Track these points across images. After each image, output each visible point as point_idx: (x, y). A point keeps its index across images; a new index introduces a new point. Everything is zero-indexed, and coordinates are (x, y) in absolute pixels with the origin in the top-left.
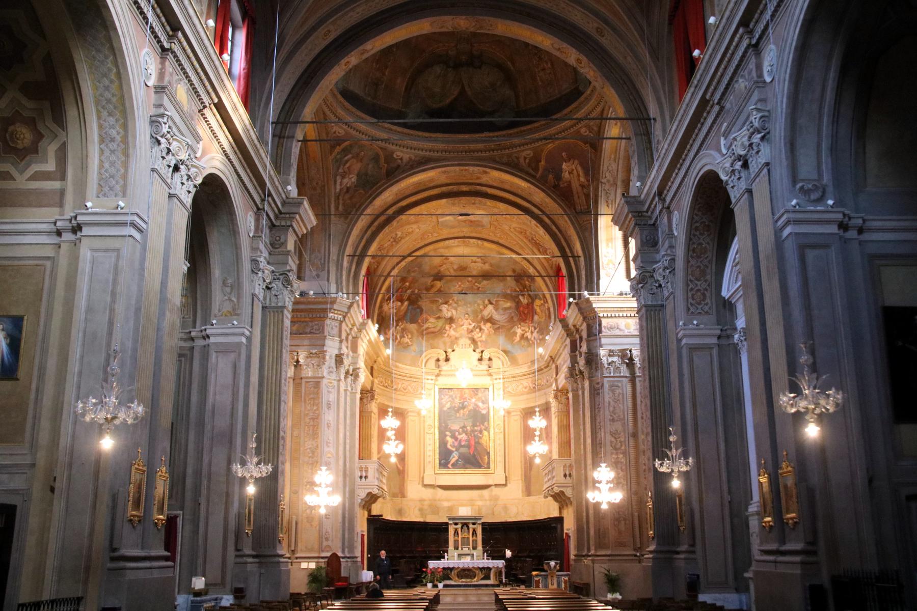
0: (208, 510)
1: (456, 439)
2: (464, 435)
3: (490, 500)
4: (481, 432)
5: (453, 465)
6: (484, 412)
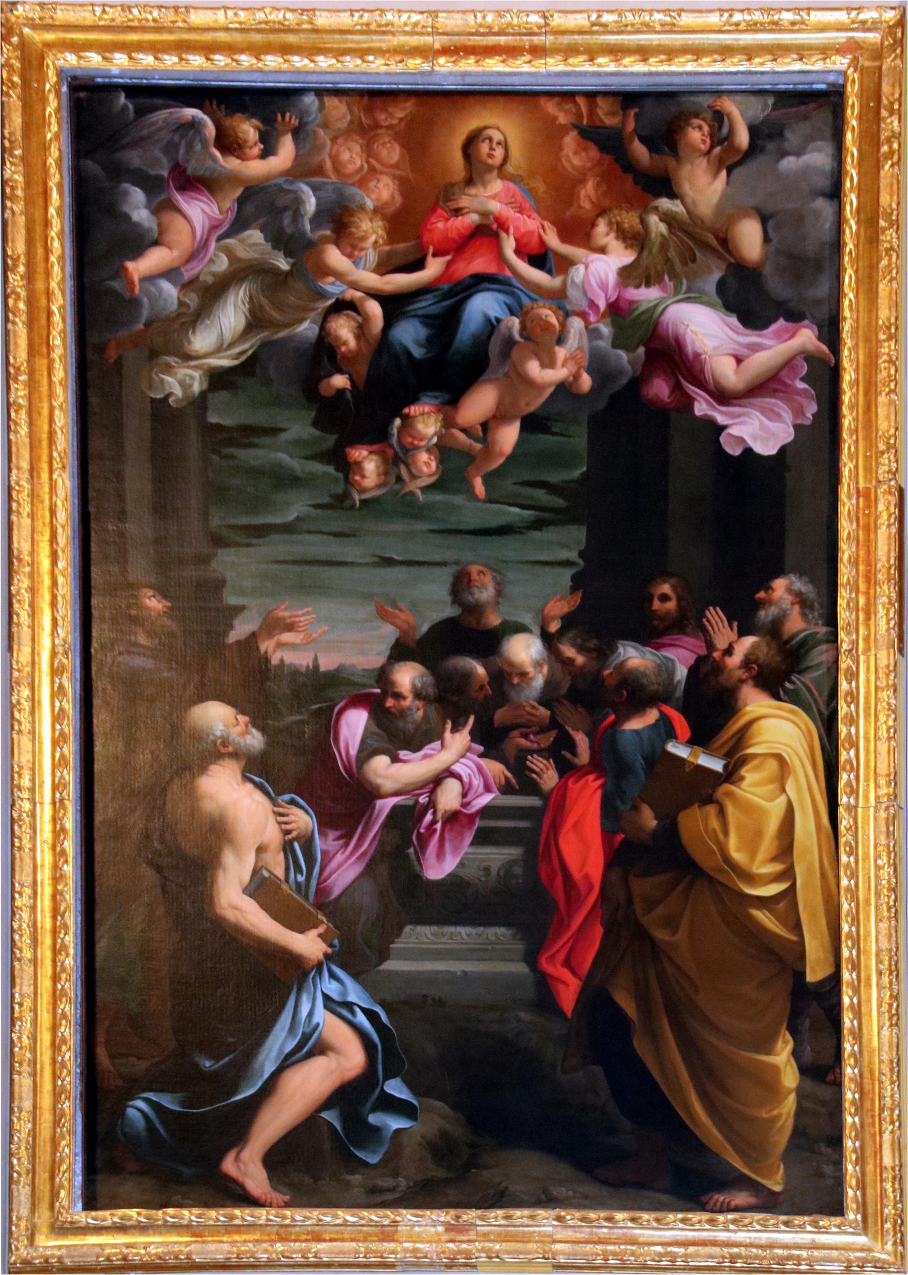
0: (34, 745)
1: (341, 798)
2: (455, 748)
3: (377, 126)
4: (709, 708)
5: (282, 1159)
6: (760, 431)
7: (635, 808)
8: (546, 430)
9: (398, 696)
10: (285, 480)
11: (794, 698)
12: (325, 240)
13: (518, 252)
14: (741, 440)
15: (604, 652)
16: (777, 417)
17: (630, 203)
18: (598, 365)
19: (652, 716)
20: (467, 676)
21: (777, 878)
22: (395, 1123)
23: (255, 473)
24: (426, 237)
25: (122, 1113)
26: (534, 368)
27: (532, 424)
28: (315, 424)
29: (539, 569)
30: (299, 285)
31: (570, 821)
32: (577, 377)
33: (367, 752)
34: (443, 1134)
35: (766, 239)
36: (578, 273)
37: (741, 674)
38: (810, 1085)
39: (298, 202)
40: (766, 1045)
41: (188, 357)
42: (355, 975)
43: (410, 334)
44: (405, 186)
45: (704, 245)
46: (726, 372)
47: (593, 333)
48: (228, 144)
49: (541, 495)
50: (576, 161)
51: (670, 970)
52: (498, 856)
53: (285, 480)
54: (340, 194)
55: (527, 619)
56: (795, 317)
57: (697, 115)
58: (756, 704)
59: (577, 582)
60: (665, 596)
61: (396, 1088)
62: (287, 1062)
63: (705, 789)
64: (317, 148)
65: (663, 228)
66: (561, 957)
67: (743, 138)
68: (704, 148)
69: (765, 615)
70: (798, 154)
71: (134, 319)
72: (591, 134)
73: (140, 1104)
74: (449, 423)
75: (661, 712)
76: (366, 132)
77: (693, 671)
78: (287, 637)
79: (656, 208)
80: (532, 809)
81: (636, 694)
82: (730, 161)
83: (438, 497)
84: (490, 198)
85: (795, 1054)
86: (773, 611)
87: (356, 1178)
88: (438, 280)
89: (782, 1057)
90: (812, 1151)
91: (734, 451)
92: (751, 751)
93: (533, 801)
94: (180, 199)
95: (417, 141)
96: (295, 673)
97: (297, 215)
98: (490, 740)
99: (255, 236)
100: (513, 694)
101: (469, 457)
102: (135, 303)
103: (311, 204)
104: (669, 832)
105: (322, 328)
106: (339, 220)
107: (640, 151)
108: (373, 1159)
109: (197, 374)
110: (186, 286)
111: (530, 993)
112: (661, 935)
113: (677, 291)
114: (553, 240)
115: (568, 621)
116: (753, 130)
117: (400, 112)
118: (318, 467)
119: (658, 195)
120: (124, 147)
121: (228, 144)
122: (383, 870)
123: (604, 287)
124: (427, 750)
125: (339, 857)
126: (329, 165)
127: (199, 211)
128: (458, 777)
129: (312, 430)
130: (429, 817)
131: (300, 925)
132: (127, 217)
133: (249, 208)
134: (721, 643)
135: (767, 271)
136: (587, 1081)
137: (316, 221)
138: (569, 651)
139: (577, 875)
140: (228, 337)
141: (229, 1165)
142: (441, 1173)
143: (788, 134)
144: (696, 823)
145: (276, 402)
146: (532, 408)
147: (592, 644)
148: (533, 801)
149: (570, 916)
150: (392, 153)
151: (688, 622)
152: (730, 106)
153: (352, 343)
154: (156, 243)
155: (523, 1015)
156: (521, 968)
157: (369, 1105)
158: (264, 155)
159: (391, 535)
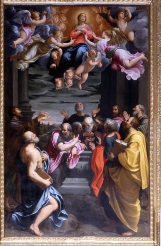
1: (53, 152)
2: (75, 141)
4: (124, 132)
5: (42, 226)
6: (133, 75)
7: (110, 153)
8: (93, 75)
9: (65, 130)
10: (44, 86)
11: (140, 130)
12: (51, 36)
13: (88, 39)
14: (130, 77)
15: (104, 121)
16: (137, 72)
17: (109, 28)
18: (103, 62)
19: (113, 134)
20: (78, 126)
21: (137, 167)
22: (63, 219)
23: (38, 84)
24: (71, 36)
25: (11, 216)
26: (91, 62)
27: (91, 74)
28: (49, 74)
29: (92, 104)
30: (46, 45)
31: (98, 156)
32: (99, 64)
33: (58, 142)
34: (73, 221)
35: (135, 36)
36: (99, 43)
37: (130, 125)
38: (143, 211)
39: (46, 29)
40: (134, 202)
41: (25, 60)
42: (56, 188)
43: (67, 55)
44: (67, 26)
45: (123, 37)
46: (127, 63)
47: (102, 55)
48: (33, 17)
49: (92, 88)
50: (99, 20)
51: (116, 187)
52: (84, 163)
53: (44, 86)
54: (54, 27)
55: (89, 114)
56: (140, 52)
57: (122, 11)
58: (133, 131)
59: (99, 106)
60: (116, 109)
61: (64, 212)
62: (43, 207)
63: (123, 149)
64: (50, 18)
65: (115, 34)
66: (95, 184)
67: (130, 16)
68: (123, 17)
69: (135, 113)
70: (141, 19)
71: (15, 53)
72: (102, 15)
73: (15, 215)
74: (75, 74)
75: (58, 142)
76: (59, 14)
77: (121, 125)
78: (43, 118)
79: (114, 30)
80: (90, 154)
81: (110, 130)
82: (128, 20)
83: (73, 89)
84: (83, 28)
85: (140, 204)
86: (136, 112)
87: (56, 230)
88: (73, 44)
89: (138, 205)
90: (143, 224)
91: (129, 79)
92: (132, 141)
93: (90, 152)
94: (24, 28)
95: (69, 16)
96: (45, 125)
97: (46, 32)
98: (82, 139)
99: (38, 36)
100: (86, 130)
101: (78, 81)
102: (15, 49)
103: (49, 29)
104: (116, 158)
105: (51, 54)
106: (54, 32)
107: (111, 18)
108: (59, 226)
109: (27, 64)
110: (25, 46)
111: (90, 192)
112: (115, 180)
113: (118, 46)
114: (95, 36)
115: (98, 114)
116: (132, 14)
117: (66, 11)
118: (50, 83)
119: (114, 27)
120: (15, 18)
121: (33, 17)
122: (61, 167)
123: (104, 45)
124: (70, 141)
125: (53, 164)
126: (52, 21)
127: (28, 31)
128: (76, 147)
129: (48, 75)
130: (70, 155)
131: (45, 178)
132: (14, 32)
133: (37, 30)
134: (126, 119)
135: (135, 42)
136: (100, 210)
137: (50, 33)
138: (97, 121)
139: (99, 168)
140: (33, 56)
141: (31, 227)
142: (72, 229)
143: (139, 15)
144: (121, 156)
145: (42, 69)
146: (91, 70)
147: (102, 119)
148: (90, 152)
149: (97, 176)
150: (64, 19)
151: (120, 114)
152: (128, 9)
153: (56, 57)
154: (19, 37)
155: (88, 197)
156: (88, 187)
157: (58, 215)
158: (40, 19)
159: (63, 97)
